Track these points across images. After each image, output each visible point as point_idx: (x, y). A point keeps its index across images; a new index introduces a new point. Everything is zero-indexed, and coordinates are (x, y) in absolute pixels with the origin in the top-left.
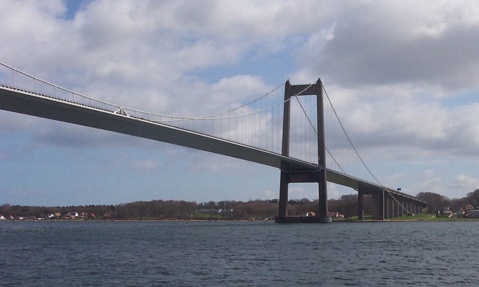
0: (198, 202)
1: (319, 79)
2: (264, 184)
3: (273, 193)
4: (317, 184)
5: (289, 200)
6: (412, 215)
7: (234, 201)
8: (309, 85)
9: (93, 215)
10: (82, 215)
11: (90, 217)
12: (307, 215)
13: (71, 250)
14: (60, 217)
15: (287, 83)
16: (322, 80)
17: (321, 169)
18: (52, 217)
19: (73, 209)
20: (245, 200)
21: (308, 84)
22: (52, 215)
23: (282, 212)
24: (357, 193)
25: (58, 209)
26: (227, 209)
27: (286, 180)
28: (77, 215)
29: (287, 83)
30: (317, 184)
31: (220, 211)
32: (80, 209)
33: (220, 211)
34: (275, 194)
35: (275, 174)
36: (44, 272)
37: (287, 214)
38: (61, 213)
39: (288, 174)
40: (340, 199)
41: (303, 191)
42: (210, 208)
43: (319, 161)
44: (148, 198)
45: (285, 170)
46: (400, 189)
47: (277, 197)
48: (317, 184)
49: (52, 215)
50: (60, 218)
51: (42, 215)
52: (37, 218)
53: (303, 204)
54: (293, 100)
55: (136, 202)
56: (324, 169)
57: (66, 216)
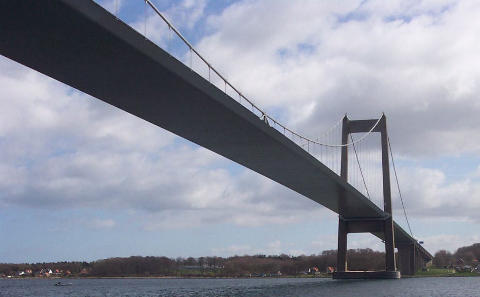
5: (348, 248)
6: (427, 270)
9: (69, 272)
10: (56, 272)
11: (65, 274)
14: (31, 274)
15: (345, 119)
17: (387, 217)
18: (22, 275)
19: (46, 266)
22: (23, 273)
23: (340, 265)
25: (25, 267)
27: (345, 228)
28: (51, 272)
29: (345, 119)
32: (54, 266)
35: (331, 219)
37: (346, 270)
38: (32, 271)
39: (347, 223)
40: (321, 254)
41: (364, 241)
42: (190, 264)
44: (126, 254)
45: (343, 217)
46: (422, 243)
47: (335, 247)
49: (23, 273)
50: (32, 275)
51: (11, 272)
52: (7, 275)
53: (366, 255)
54: (355, 137)
55: (112, 259)
57: (40, 274)
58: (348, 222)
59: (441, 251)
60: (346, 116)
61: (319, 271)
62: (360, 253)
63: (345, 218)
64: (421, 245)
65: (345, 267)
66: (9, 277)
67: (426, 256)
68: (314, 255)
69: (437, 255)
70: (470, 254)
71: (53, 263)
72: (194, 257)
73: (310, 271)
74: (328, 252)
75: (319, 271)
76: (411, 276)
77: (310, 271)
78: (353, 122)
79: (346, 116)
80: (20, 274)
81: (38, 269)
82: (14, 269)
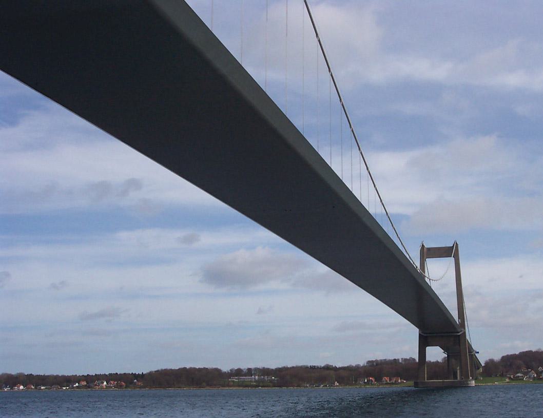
5: (427, 360)
10: (111, 384)
17: (463, 332)
19: (99, 378)
22: (77, 384)
25: (78, 379)
27: (424, 342)
28: (105, 383)
38: (86, 382)
41: (435, 354)
47: (416, 357)
49: (77, 384)
58: (426, 337)
59: (490, 360)
60: (423, 245)
61: (375, 381)
62: (403, 363)
63: (425, 333)
64: (476, 354)
65: (425, 376)
66: (64, 388)
67: (476, 363)
68: (358, 365)
69: (487, 363)
70: (519, 362)
71: (132, 373)
72: (242, 368)
73: (366, 381)
74: (372, 361)
75: (375, 381)
76: (426, 388)
77: (366, 381)
78: (429, 249)
79: (423, 245)
80: (74, 386)
81: (91, 380)
82: (68, 380)
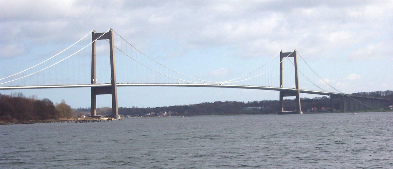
0: (246, 102)
1: (282, 51)
2: (275, 96)
3: (278, 98)
4: (111, 95)
7: (271, 100)
8: (291, 53)
12: (312, 109)
13: (80, 149)
16: (297, 51)
20: (213, 102)
21: (290, 52)
22: (149, 114)
24: (330, 97)
26: (265, 106)
28: (166, 113)
30: (111, 95)
31: (260, 108)
33: (260, 108)
34: (87, 105)
36: (264, 142)
43: (296, 87)
48: (111, 95)
49: (149, 114)
56: (298, 91)
